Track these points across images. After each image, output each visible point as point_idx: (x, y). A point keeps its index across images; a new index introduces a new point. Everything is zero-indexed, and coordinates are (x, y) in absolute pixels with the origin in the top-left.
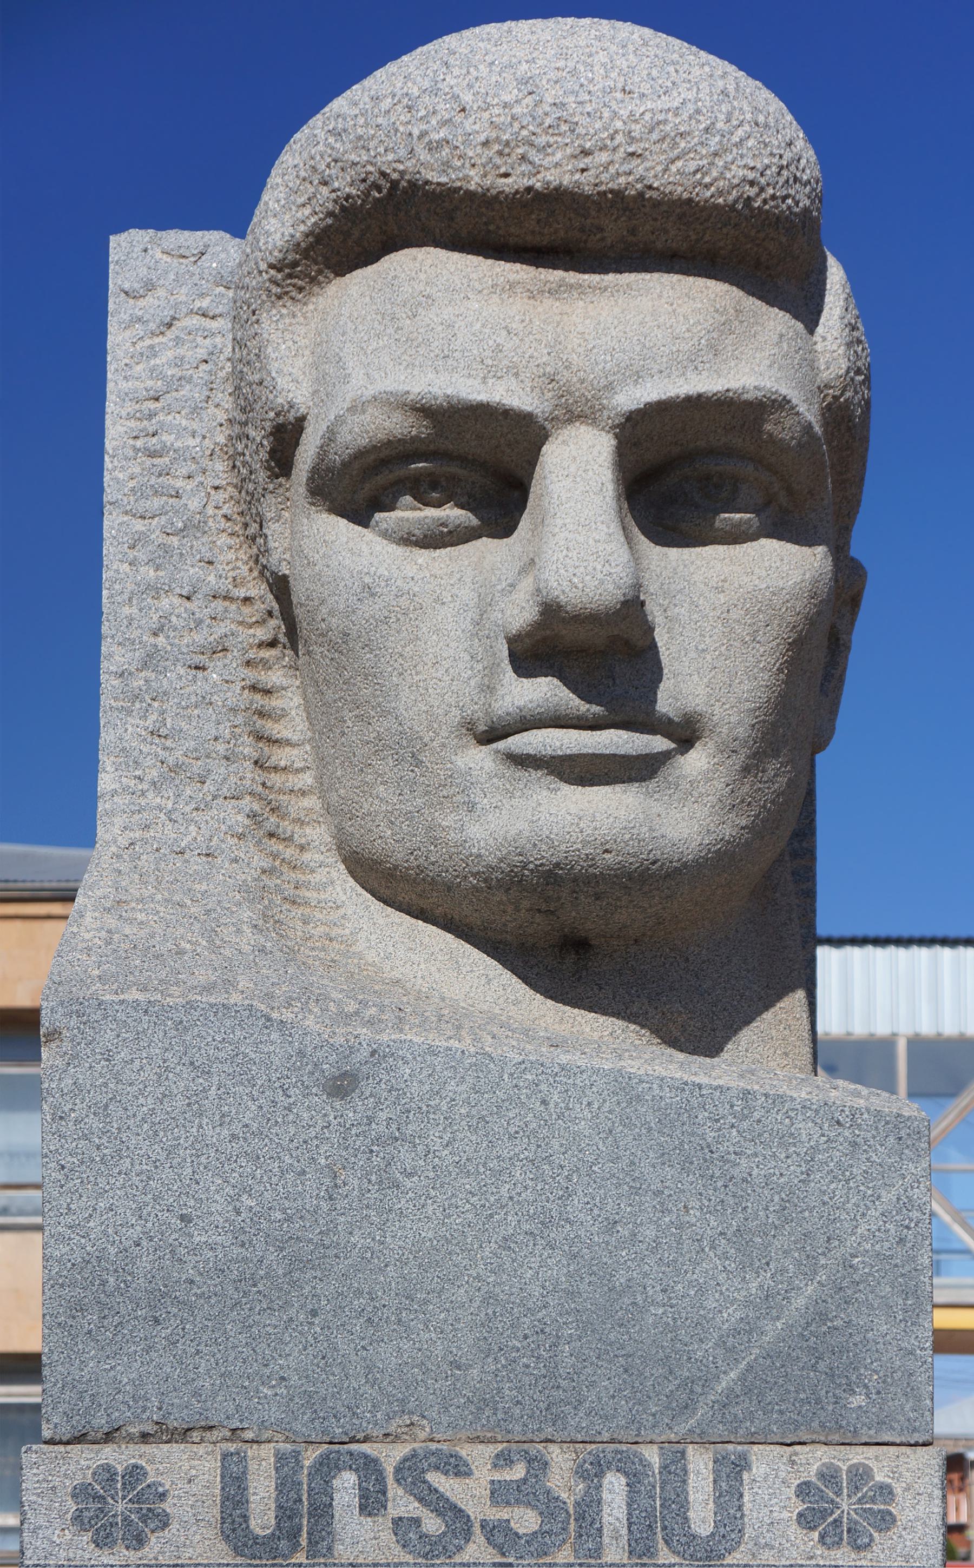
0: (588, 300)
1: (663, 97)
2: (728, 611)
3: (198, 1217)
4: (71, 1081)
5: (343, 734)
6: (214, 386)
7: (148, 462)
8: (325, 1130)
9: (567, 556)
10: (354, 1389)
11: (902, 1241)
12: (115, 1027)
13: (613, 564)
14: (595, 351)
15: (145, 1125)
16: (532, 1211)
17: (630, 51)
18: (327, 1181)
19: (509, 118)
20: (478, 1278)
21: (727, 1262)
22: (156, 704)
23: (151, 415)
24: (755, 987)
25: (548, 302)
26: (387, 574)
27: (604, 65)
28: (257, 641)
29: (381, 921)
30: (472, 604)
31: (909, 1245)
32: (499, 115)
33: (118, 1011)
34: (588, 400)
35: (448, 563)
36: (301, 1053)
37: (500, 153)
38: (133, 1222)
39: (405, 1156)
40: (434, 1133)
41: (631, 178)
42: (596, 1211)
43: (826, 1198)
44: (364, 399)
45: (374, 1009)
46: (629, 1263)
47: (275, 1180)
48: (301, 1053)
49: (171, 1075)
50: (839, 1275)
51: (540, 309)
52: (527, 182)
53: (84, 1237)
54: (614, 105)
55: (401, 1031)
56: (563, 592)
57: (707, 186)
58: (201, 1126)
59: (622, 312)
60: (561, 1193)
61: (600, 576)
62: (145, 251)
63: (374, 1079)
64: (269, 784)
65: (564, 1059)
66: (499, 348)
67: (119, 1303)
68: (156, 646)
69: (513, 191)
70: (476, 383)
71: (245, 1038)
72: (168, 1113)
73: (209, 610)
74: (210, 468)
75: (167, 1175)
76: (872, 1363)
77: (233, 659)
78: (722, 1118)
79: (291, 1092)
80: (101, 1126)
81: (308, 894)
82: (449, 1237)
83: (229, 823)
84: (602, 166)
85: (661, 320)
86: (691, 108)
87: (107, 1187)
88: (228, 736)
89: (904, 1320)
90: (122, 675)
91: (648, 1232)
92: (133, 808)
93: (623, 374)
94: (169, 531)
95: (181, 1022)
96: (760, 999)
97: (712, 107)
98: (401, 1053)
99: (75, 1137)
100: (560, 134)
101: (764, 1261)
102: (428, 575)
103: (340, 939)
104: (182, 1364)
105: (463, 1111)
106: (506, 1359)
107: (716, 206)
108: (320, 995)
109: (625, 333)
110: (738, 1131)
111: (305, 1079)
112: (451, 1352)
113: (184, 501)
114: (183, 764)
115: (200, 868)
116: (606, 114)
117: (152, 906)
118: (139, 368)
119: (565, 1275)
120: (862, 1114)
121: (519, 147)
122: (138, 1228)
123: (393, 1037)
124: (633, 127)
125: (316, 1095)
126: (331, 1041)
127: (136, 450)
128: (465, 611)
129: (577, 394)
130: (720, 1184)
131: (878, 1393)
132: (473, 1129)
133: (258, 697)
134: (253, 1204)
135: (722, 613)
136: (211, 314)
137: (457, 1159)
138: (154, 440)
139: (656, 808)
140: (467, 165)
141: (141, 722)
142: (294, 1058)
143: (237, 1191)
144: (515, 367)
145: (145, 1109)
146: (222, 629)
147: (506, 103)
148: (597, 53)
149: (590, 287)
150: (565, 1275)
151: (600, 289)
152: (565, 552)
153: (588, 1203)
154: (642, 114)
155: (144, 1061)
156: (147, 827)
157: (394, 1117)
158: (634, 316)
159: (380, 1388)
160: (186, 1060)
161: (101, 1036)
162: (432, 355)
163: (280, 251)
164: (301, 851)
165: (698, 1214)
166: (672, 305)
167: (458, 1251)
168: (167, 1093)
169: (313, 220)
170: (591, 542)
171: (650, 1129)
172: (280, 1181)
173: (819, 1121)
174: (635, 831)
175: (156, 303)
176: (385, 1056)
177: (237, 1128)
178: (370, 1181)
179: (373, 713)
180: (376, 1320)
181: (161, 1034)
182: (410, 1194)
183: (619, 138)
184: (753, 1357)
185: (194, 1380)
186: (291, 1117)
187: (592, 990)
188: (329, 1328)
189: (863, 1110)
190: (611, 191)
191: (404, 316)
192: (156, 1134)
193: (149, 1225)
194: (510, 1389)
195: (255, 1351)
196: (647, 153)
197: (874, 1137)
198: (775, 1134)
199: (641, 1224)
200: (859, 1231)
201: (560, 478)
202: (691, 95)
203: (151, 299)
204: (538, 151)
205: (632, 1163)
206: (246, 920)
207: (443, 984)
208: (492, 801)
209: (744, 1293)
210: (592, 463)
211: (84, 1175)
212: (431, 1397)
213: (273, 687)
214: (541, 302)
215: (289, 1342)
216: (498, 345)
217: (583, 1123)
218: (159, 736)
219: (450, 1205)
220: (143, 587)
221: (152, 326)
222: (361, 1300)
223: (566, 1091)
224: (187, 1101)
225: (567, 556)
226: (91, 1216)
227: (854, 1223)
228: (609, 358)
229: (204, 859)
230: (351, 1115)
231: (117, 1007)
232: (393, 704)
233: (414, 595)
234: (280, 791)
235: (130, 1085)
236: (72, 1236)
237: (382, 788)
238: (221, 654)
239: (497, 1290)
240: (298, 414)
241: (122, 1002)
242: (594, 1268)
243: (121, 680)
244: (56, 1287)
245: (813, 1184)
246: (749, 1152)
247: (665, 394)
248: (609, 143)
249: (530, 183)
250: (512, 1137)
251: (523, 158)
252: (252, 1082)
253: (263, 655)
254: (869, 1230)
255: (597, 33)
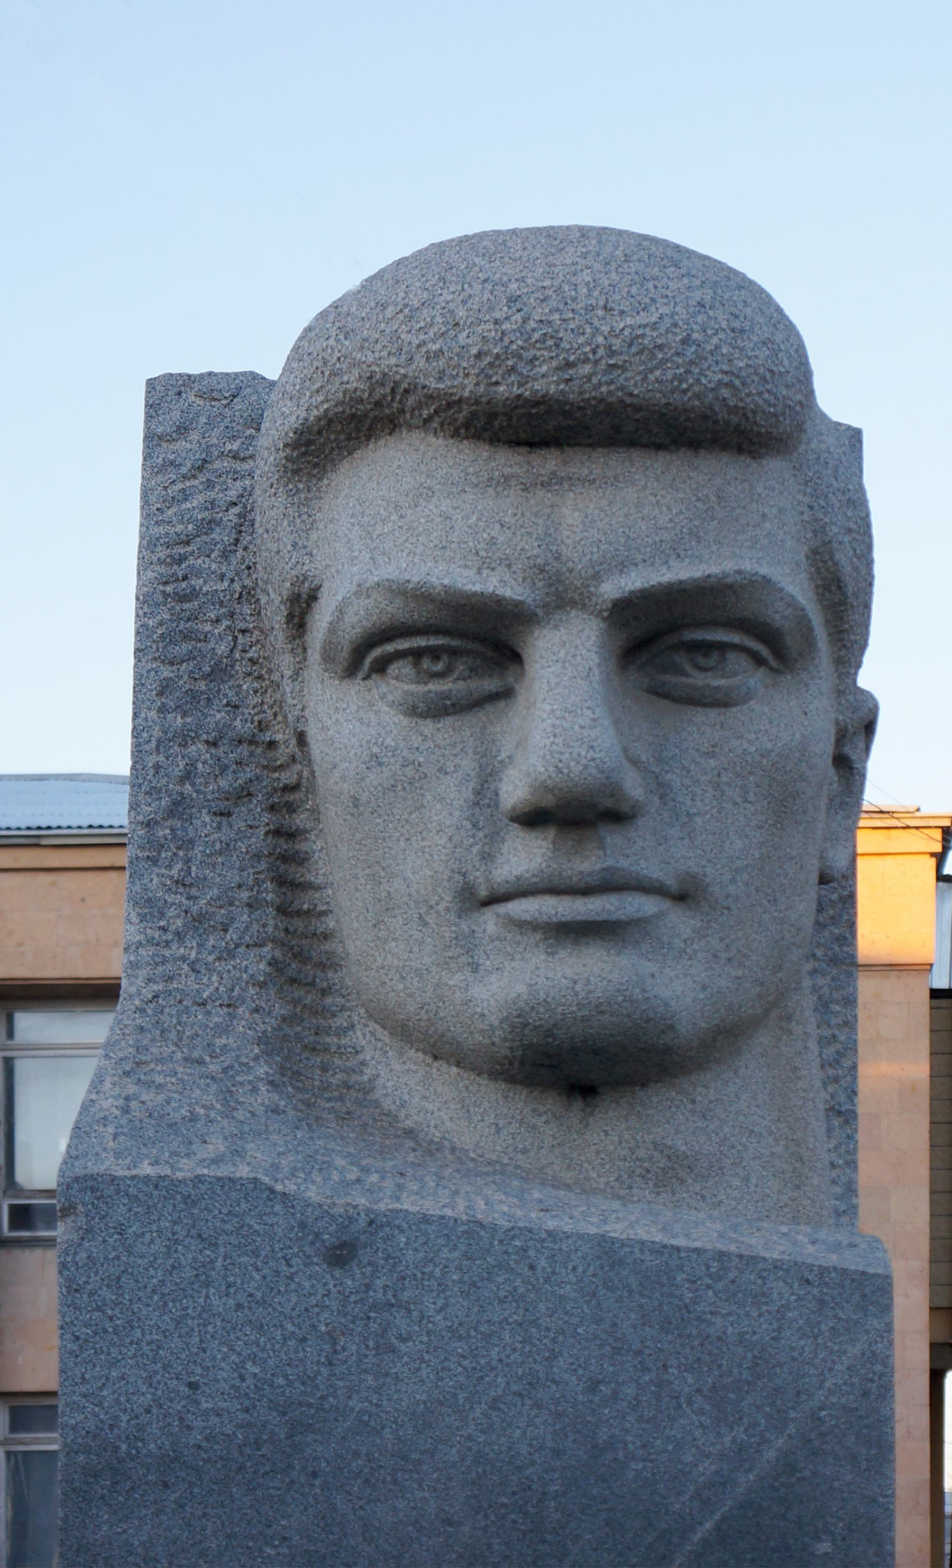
0: (578, 491)
1: (641, 313)
2: (719, 775)
3: (205, 1384)
4: (85, 1255)
5: (357, 889)
6: (243, 528)
7: (178, 608)
8: (326, 1299)
9: (553, 743)
10: (352, 1547)
11: (865, 1394)
12: (127, 1201)
13: (597, 750)
14: (583, 543)
15: (156, 1297)
16: (520, 1373)
17: (613, 268)
18: (327, 1347)
19: (499, 333)
20: (469, 1438)
21: (703, 1418)
22: (181, 853)
23: (181, 559)
24: (765, 1122)
25: (540, 493)
26: (393, 744)
27: (588, 284)
28: (281, 785)
29: (398, 1067)
30: (473, 774)
31: (873, 1397)
32: (490, 330)
33: (129, 1186)
34: (577, 588)
35: (452, 733)
36: (302, 1225)
37: (491, 365)
38: (144, 1390)
39: (400, 1320)
40: (427, 1300)
41: (612, 387)
42: (581, 1372)
43: (795, 1354)
44: (368, 585)
45: (376, 1175)
46: (611, 1421)
47: (277, 1347)
48: (302, 1225)
49: (180, 1248)
50: (807, 1428)
51: (533, 502)
52: (516, 391)
53: (97, 1405)
54: (596, 322)
55: (398, 1199)
56: (550, 777)
57: (684, 392)
58: (207, 1297)
59: (609, 505)
60: (547, 1355)
61: (584, 761)
62: (179, 394)
63: (372, 1248)
64: (291, 929)
65: (551, 1224)
66: (492, 541)
67: (130, 1469)
68: (182, 794)
69: (504, 398)
70: (471, 573)
71: (250, 1210)
72: (177, 1284)
73: (234, 755)
74: (238, 611)
75: (176, 1343)
76: (838, 1511)
77: (256, 805)
78: (699, 1279)
79: (293, 1262)
80: (114, 1297)
81: (328, 1039)
82: (442, 1399)
83: (251, 972)
84: (585, 377)
85: (646, 512)
86: (668, 322)
87: (120, 1357)
88: (251, 882)
89: (867, 1469)
90: (148, 825)
91: (629, 1391)
92: (157, 959)
93: (610, 564)
94: (197, 676)
95: (189, 1196)
96: (770, 1134)
97: (688, 319)
98: (397, 1222)
99: (89, 1309)
100: (546, 348)
101: (737, 1416)
102: (432, 746)
103: (357, 1087)
104: (190, 1526)
105: (455, 1277)
106: (496, 1515)
107: (692, 409)
108: (324, 1162)
109: (611, 525)
110: (714, 1292)
111: (307, 1248)
112: (443, 1510)
113: (212, 645)
114: (207, 912)
115: (221, 1020)
116: (588, 330)
117: (171, 1066)
118: (170, 512)
119: (551, 1433)
120: (829, 1273)
121: (508, 359)
122: (149, 1396)
123: (390, 1207)
124: (614, 341)
125: (317, 1264)
126: (332, 1212)
127: (165, 595)
128: (467, 781)
129: (567, 582)
130: (696, 1343)
131: (844, 1539)
132: (466, 1295)
133: (282, 841)
134: (257, 1371)
135: (713, 777)
136: (242, 455)
137: (449, 1324)
138: (184, 585)
139: (648, 967)
140: (461, 374)
141: (166, 872)
142: (296, 1229)
143: (242, 1358)
144: (506, 559)
145: (155, 1280)
146: (249, 772)
147: (496, 320)
148: (582, 271)
149: (579, 480)
150: (551, 1433)
151: (589, 481)
152: (552, 739)
153: (573, 1364)
154: (623, 329)
155: (155, 1235)
156: (170, 979)
157: (390, 1284)
158: (620, 508)
159: (377, 1546)
160: (194, 1232)
161: (115, 1211)
162: (432, 545)
163: (295, 433)
164: (323, 995)
165: (676, 1372)
166: (656, 496)
167: (451, 1413)
168: (176, 1264)
169: (325, 406)
170: (576, 727)
171: (631, 1292)
172: (282, 1347)
173: (789, 1281)
174: (627, 993)
175: (189, 446)
176: (382, 1226)
177: (242, 1298)
178: (367, 1347)
179: (383, 874)
180: (373, 1481)
181: (171, 1207)
182: (406, 1359)
183: (601, 352)
184: (727, 1508)
185: (201, 1541)
186: (293, 1286)
187: (599, 1135)
188: (328, 1489)
189: (831, 1269)
190: (594, 398)
191: (407, 505)
192: (165, 1304)
193: (159, 1393)
194: (499, 1544)
195: (259, 1513)
196: (628, 364)
197: (840, 1294)
198: (749, 1293)
199: (623, 1383)
200: (827, 1385)
201: (550, 663)
202: (666, 310)
203: (184, 443)
204: (526, 363)
205: (614, 1325)
206: (262, 1076)
207: (455, 1134)
208: (495, 963)
209: (719, 1447)
210: (581, 647)
211: (97, 1346)
212: (424, 1554)
213: (296, 830)
214: (534, 494)
215: (291, 1504)
216: (492, 538)
217: (568, 1287)
218: (184, 885)
219: (443, 1369)
220: (170, 735)
221: (184, 470)
222: (359, 1462)
223: (553, 1256)
224: (195, 1272)
225: (553, 743)
226: (104, 1385)
227: (822, 1377)
228: (595, 550)
229: (226, 1010)
230: (350, 1283)
231: (129, 1183)
232: (401, 867)
233: (419, 765)
234: (304, 936)
235: (141, 1257)
236: (87, 1405)
237: (393, 944)
238: (245, 800)
239: (487, 1450)
240: (312, 586)
241: (133, 1178)
242: (579, 1426)
243: (147, 830)
244: (72, 1454)
245: (783, 1342)
246: (724, 1311)
247: (648, 582)
248: (591, 356)
249: (519, 392)
250: (502, 1301)
251: (513, 369)
252: (256, 1253)
253: (287, 799)
254: (835, 1384)
255: (584, 250)
